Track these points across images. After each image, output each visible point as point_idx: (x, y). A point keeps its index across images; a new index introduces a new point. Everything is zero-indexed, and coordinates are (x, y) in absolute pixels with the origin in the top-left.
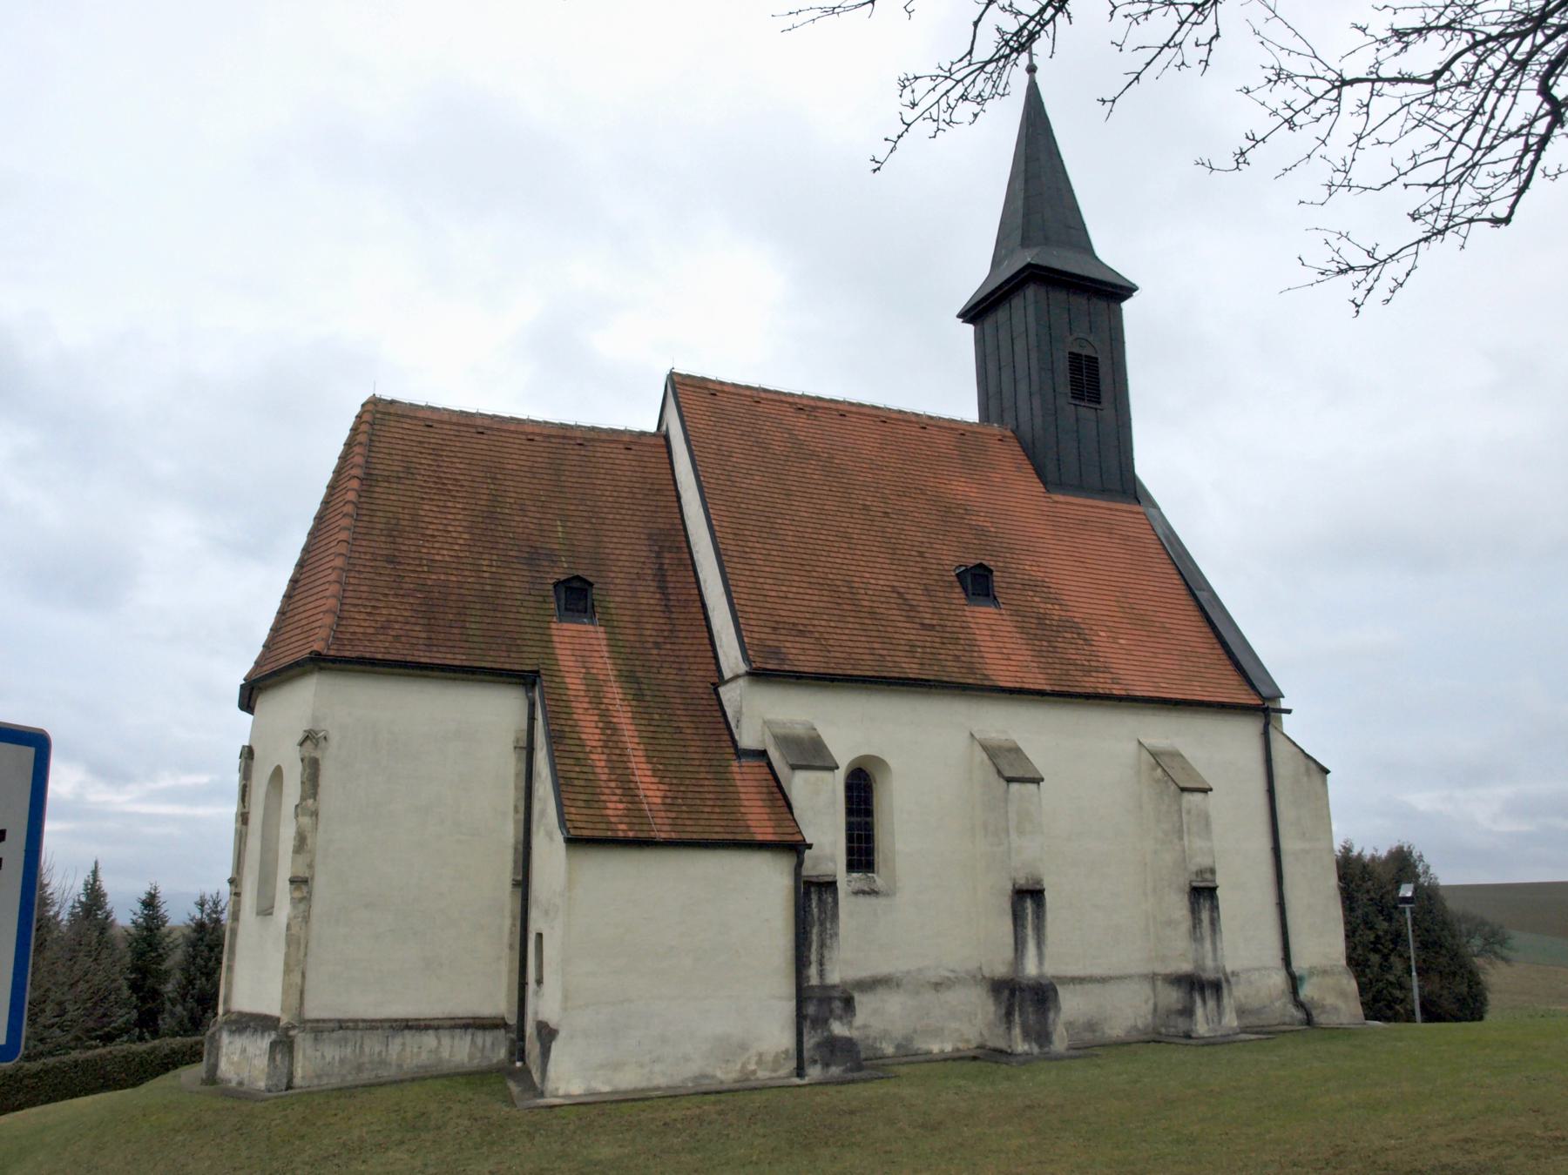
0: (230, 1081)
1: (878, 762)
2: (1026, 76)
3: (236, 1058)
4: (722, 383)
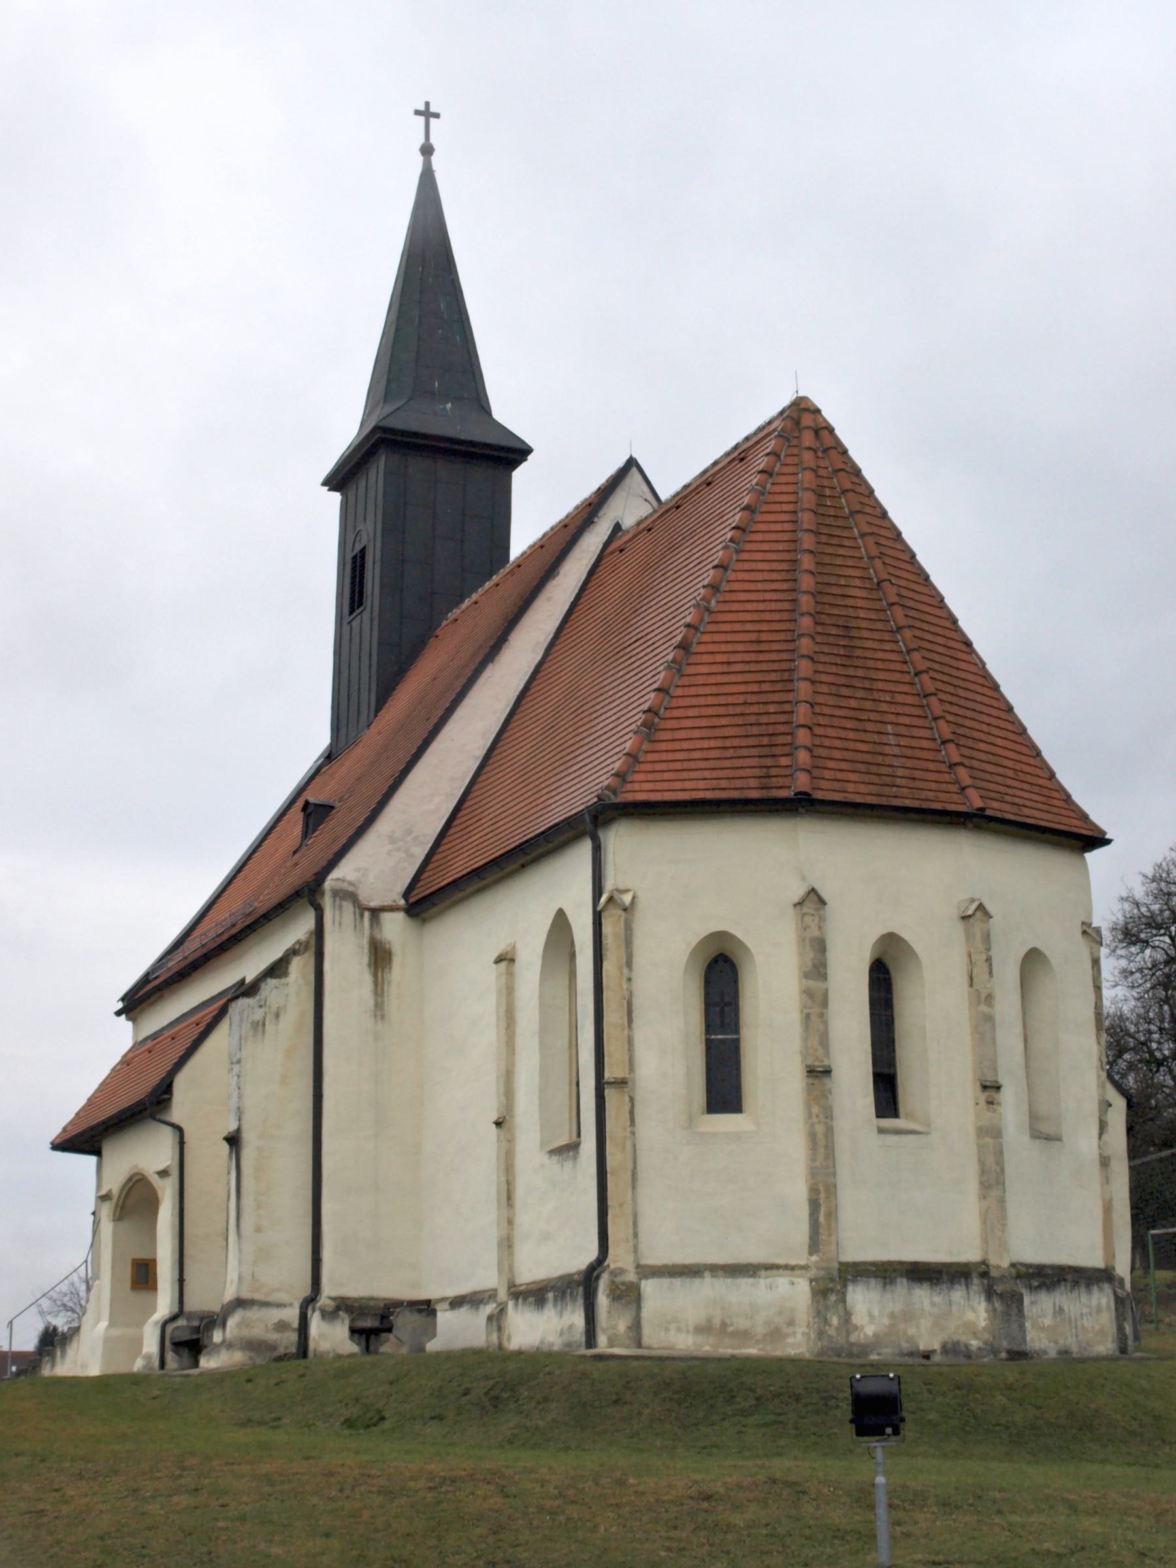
0: (1045, 1352)
1: (721, 937)
2: (420, 159)
3: (1048, 1321)
4: (677, 494)
